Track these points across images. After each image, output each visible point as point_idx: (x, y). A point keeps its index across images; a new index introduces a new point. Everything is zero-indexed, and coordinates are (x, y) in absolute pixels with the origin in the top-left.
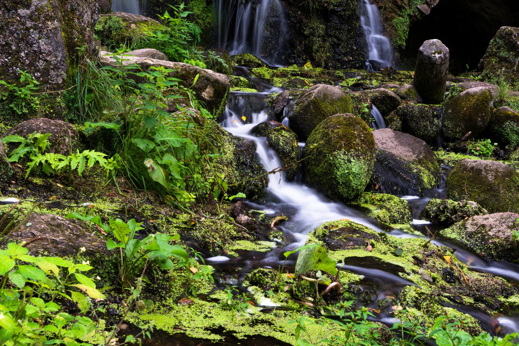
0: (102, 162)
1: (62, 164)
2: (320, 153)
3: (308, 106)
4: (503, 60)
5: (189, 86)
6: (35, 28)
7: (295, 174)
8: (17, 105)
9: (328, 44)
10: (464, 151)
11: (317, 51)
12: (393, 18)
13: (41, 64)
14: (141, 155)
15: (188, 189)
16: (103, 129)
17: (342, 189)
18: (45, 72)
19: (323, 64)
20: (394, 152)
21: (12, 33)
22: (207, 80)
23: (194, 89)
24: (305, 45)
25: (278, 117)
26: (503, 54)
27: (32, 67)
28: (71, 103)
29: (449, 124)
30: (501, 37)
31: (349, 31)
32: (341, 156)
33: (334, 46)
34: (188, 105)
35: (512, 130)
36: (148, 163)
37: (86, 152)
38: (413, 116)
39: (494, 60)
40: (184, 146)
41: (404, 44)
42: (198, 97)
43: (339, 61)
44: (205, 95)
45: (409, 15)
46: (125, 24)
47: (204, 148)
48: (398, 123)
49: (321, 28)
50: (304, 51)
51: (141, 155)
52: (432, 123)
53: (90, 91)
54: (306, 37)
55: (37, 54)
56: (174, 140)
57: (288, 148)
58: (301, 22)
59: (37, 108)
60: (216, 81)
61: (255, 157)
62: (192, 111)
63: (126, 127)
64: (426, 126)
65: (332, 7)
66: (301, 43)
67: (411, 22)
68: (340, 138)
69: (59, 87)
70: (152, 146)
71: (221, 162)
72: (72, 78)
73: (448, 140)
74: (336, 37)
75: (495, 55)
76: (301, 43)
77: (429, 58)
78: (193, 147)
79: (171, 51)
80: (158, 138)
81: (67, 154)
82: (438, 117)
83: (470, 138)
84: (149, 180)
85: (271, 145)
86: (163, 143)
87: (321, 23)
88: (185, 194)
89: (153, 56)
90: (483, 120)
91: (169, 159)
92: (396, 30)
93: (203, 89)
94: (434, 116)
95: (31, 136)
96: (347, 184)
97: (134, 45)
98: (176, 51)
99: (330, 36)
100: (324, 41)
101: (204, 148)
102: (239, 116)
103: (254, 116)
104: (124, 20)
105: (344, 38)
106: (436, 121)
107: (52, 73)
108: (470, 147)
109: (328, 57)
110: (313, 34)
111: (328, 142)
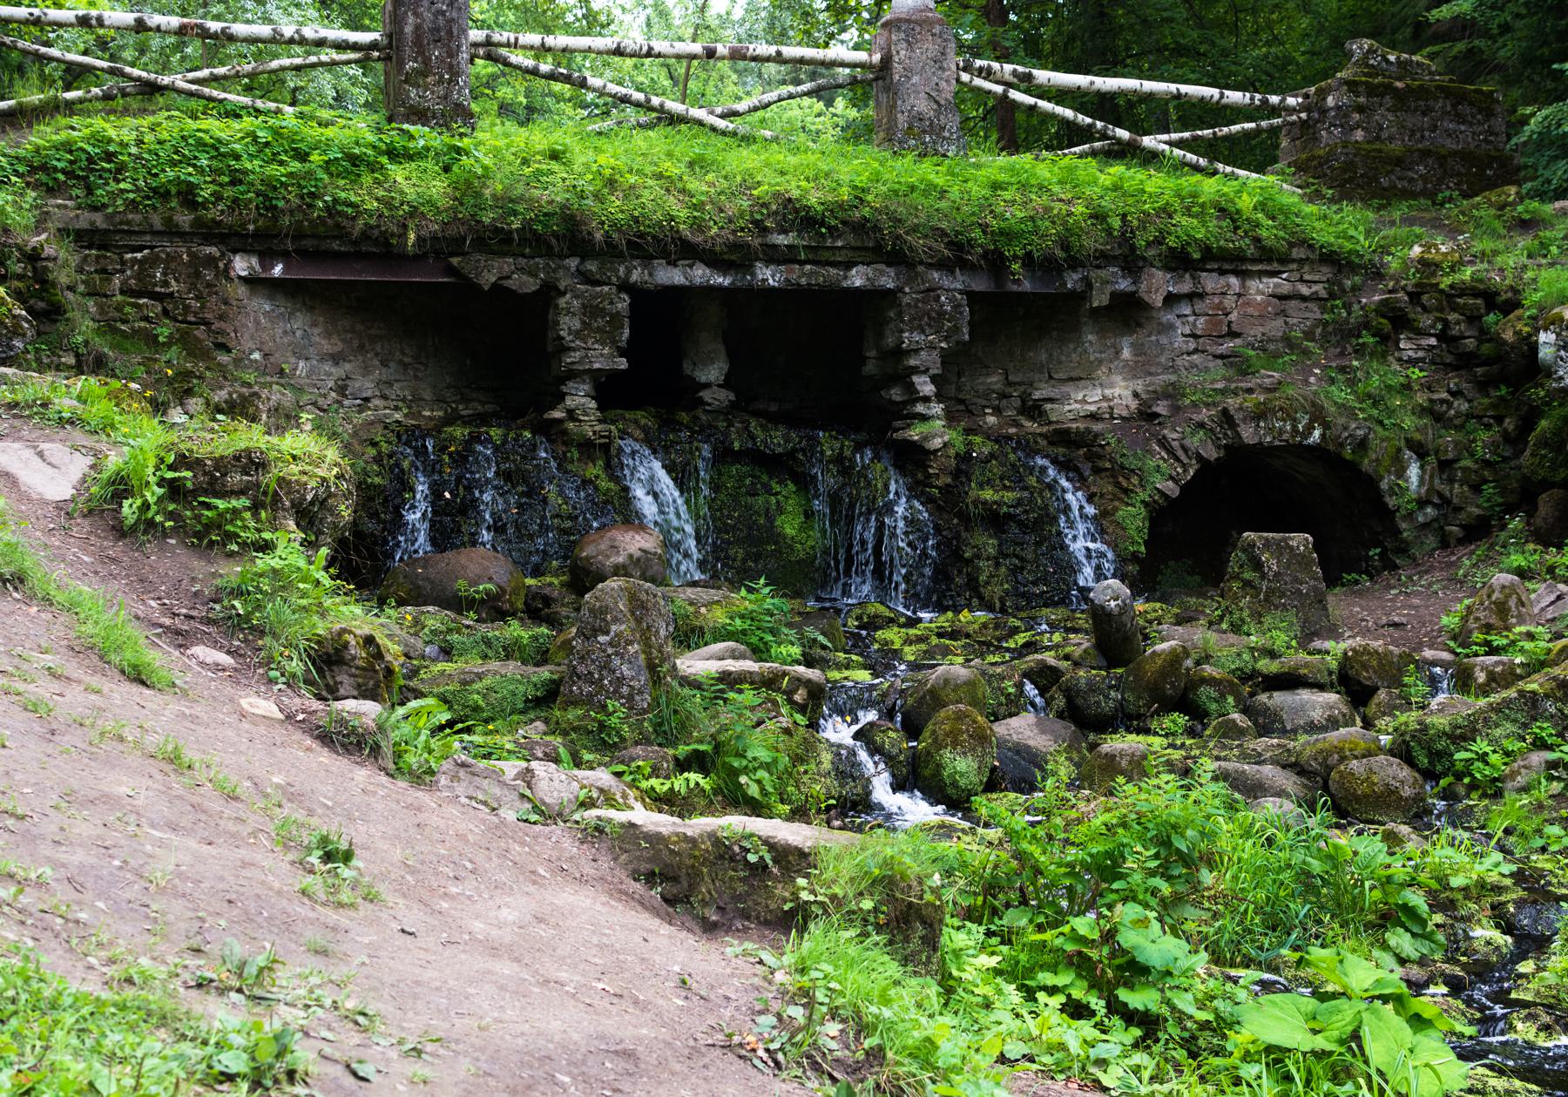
0: (702, 782)
1: (665, 788)
2: (928, 753)
3: (924, 697)
4: (1248, 584)
5: (778, 690)
6: (617, 654)
7: (906, 779)
8: (609, 735)
9: (1003, 569)
10: (1147, 731)
11: (987, 583)
12: (1116, 509)
13: (625, 690)
14: (735, 773)
15: (782, 801)
16: (696, 751)
17: (950, 791)
18: (630, 698)
19: (998, 605)
20: (1031, 743)
21: (593, 661)
22: (799, 681)
23: (784, 693)
24: (968, 574)
25: (889, 714)
26: (1247, 575)
27: (616, 694)
28: (658, 726)
29: (1129, 696)
30: (1244, 550)
31: (1038, 544)
32: (947, 754)
33: (1015, 571)
34: (779, 714)
35: (1209, 698)
36: (743, 779)
37: (686, 775)
38: (1079, 691)
39: (1235, 585)
40: (775, 761)
41: (1143, 549)
42: (791, 701)
43: (1023, 595)
44: (797, 698)
45: (1143, 502)
46: (691, 609)
47: (798, 759)
48: (1060, 702)
49: (991, 545)
50: (967, 584)
51: (735, 773)
52: (1107, 697)
53: (676, 712)
54: (969, 562)
55: (620, 681)
56: (764, 755)
57: (894, 751)
58: (958, 537)
59: (627, 735)
60: (809, 681)
61: (857, 765)
62: (785, 721)
63: (718, 747)
64: (1098, 703)
65: (1005, 509)
66: (960, 572)
67: (1150, 512)
68: (947, 735)
69: (645, 711)
70: (745, 763)
71: (819, 774)
72: (656, 700)
73: (1130, 717)
74: (1017, 557)
75: (1236, 577)
76: (960, 572)
77: (1103, 608)
78: (784, 760)
79: (754, 640)
80: (750, 755)
81: (667, 777)
82: (1116, 688)
83: (1157, 713)
84: (745, 795)
85: (874, 749)
86: (755, 759)
87: (990, 536)
88: (780, 806)
89: (735, 656)
90: (1173, 687)
91: (762, 774)
92: (1124, 529)
93: (795, 691)
94: (1111, 687)
95: (633, 765)
96: (955, 784)
97: (708, 637)
98: (761, 639)
99: (1006, 556)
100: (997, 565)
101: (798, 759)
102: (843, 716)
103: (860, 714)
104: (691, 604)
105: (1030, 557)
106: (1113, 694)
107: (637, 698)
108: (1154, 725)
109: (1007, 592)
110: (978, 557)
111: (935, 741)
